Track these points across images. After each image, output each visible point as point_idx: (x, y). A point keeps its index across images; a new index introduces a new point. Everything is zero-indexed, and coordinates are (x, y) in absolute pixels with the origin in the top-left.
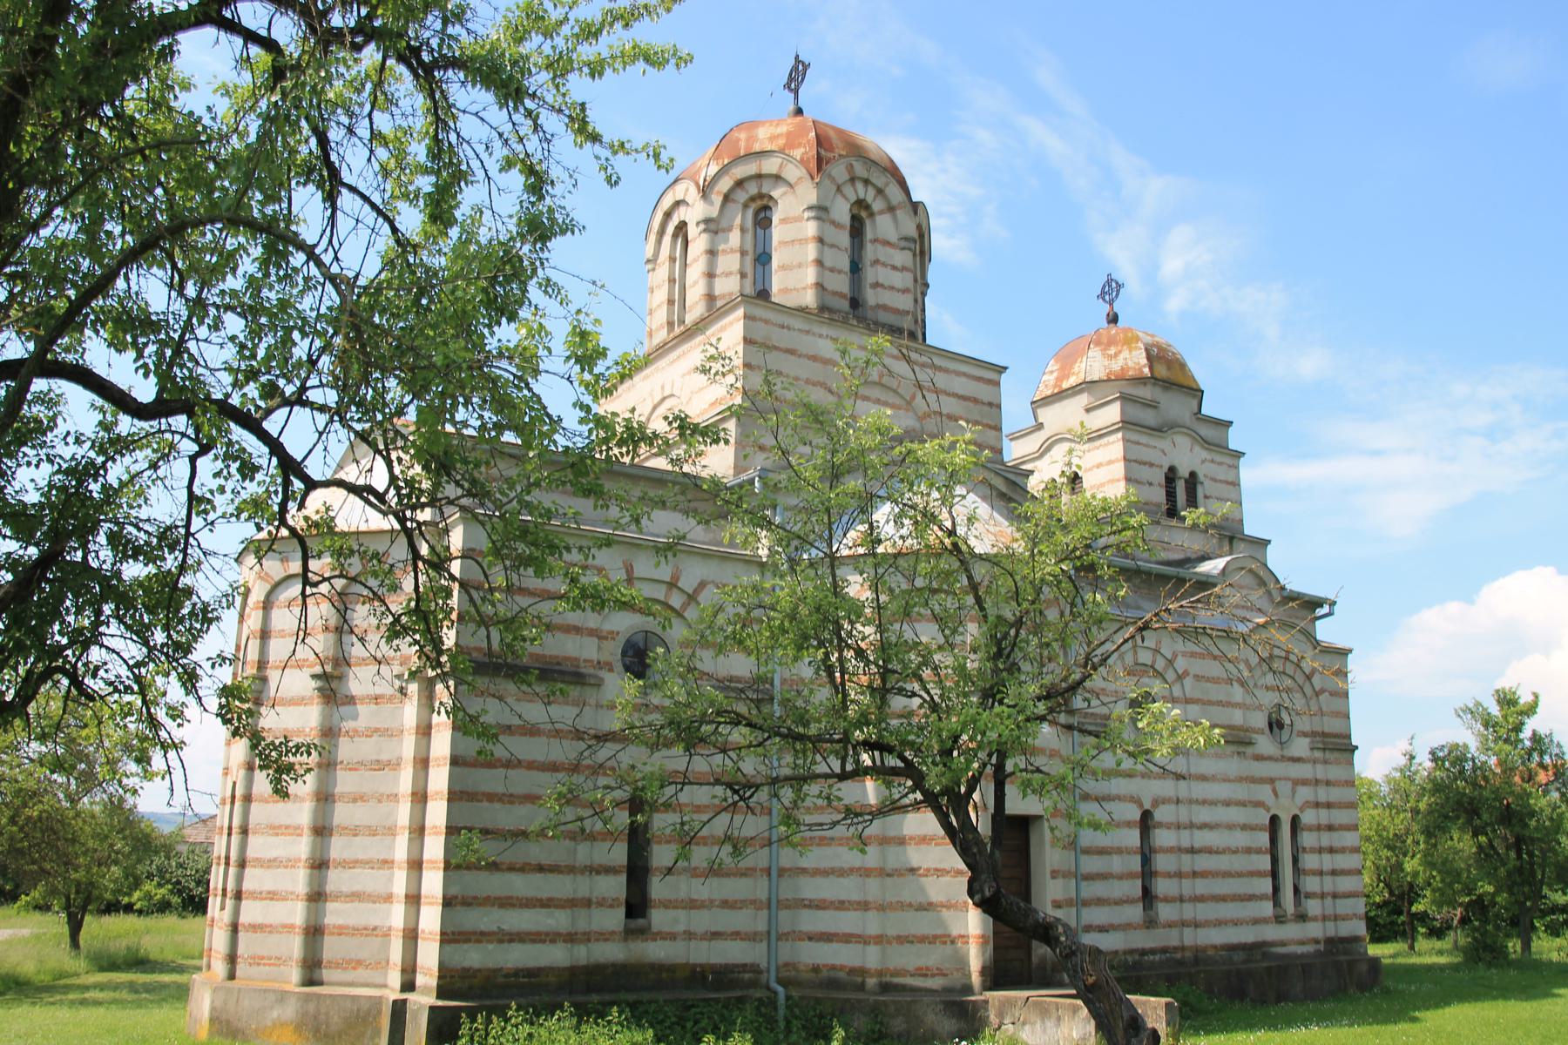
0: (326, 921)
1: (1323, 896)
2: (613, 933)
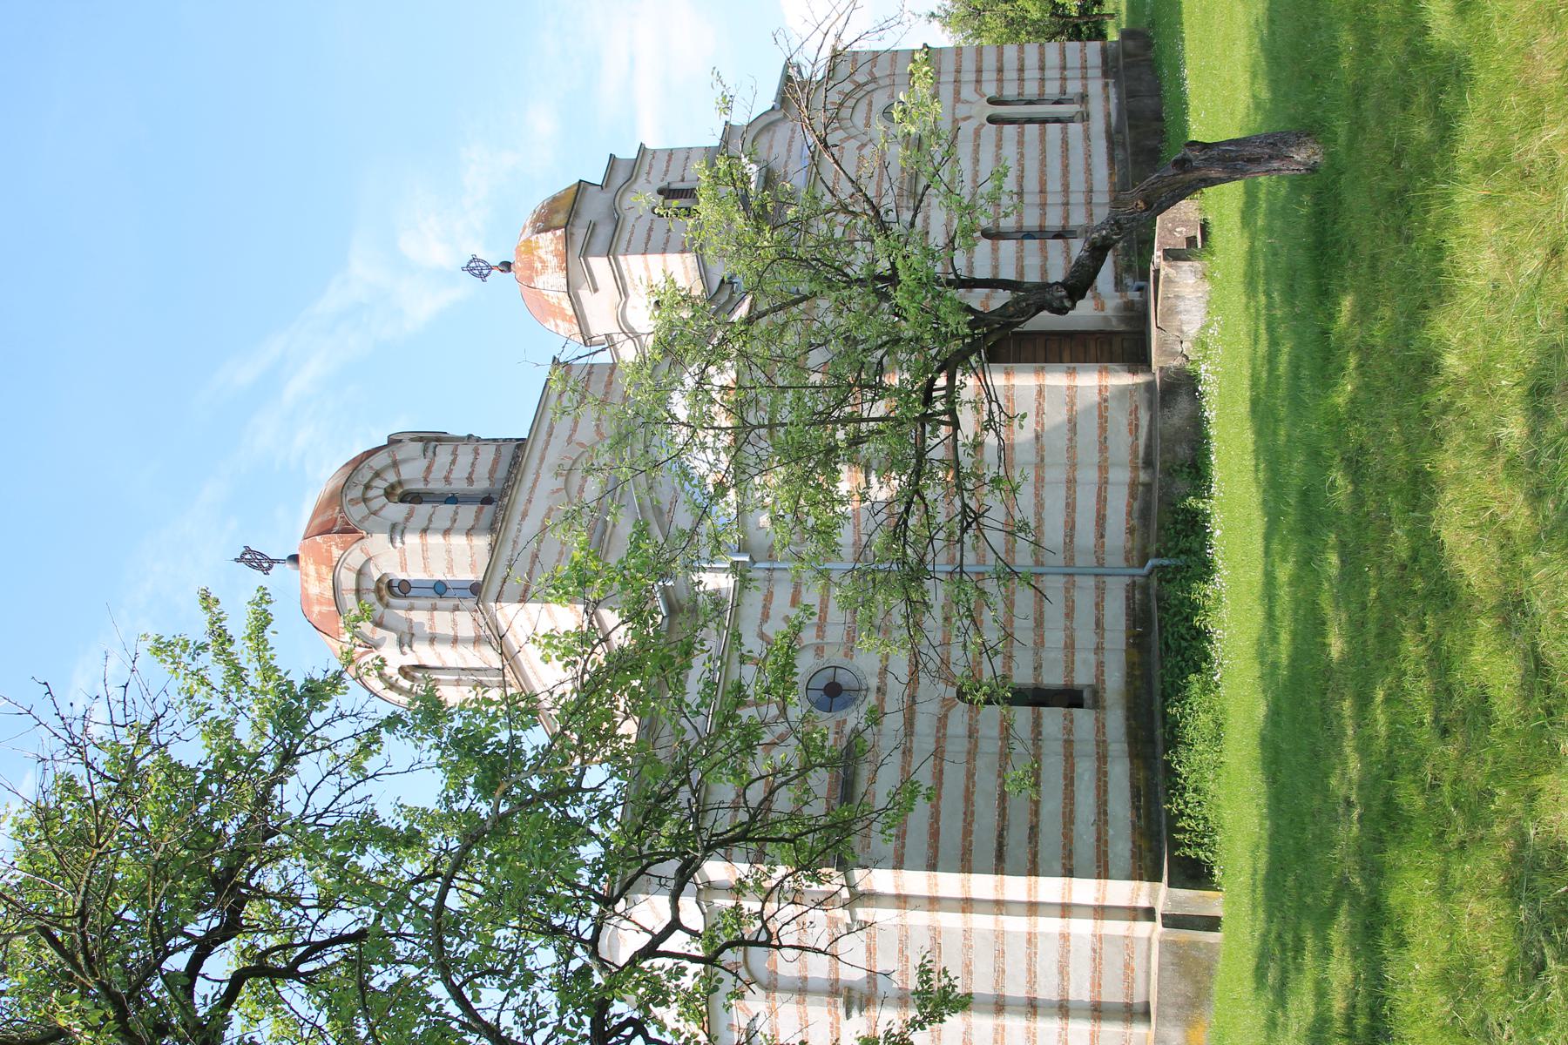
0: (1087, 999)
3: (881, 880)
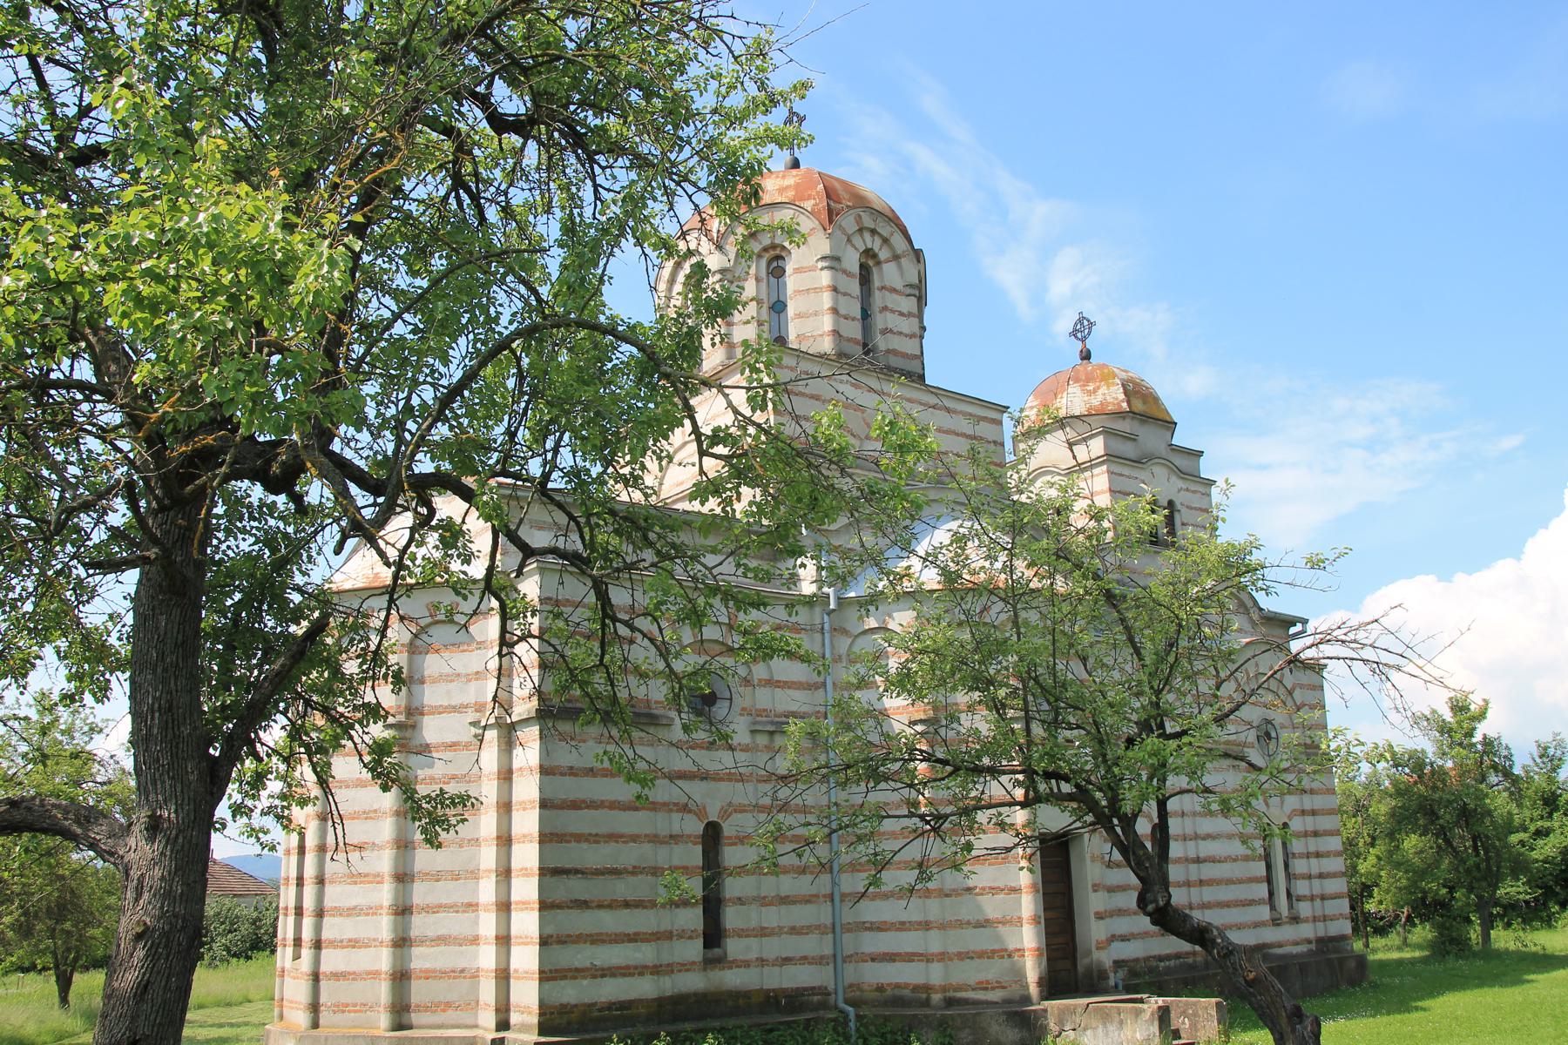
0: (413, 966)
1: (1312, 898)
2: (693, 963)
3: (528, 753)
